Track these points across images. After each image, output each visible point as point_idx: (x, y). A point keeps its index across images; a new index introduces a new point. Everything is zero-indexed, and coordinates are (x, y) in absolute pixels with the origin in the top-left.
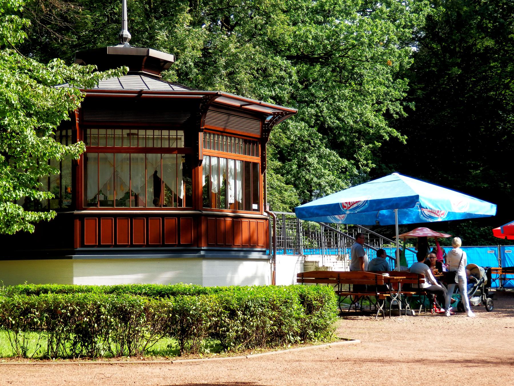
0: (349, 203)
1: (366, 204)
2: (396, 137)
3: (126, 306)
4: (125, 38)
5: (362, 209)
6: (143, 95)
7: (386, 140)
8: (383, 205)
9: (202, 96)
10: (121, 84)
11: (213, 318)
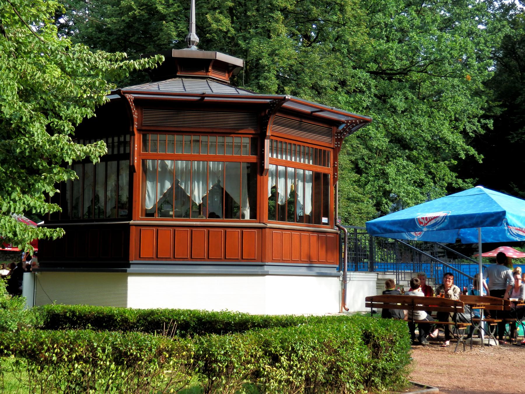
0: (426, 218)
1: (446, 221)
2: (473, 155)
3: (132, 349)
4: (192, 41)
5: (441, 226)
6: (206, 98)
7: (461, 158)
8: (465, 222)
9: (268, 101)
10: (184, 87)
11: (249, 366)
